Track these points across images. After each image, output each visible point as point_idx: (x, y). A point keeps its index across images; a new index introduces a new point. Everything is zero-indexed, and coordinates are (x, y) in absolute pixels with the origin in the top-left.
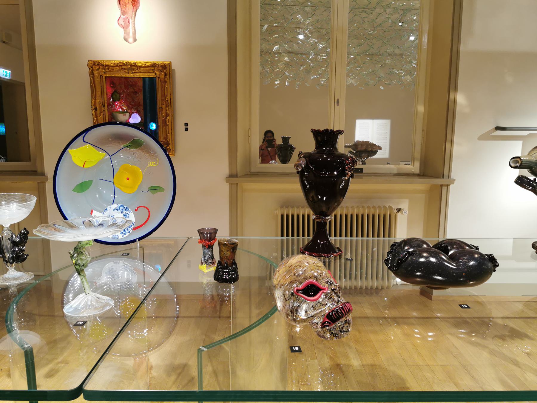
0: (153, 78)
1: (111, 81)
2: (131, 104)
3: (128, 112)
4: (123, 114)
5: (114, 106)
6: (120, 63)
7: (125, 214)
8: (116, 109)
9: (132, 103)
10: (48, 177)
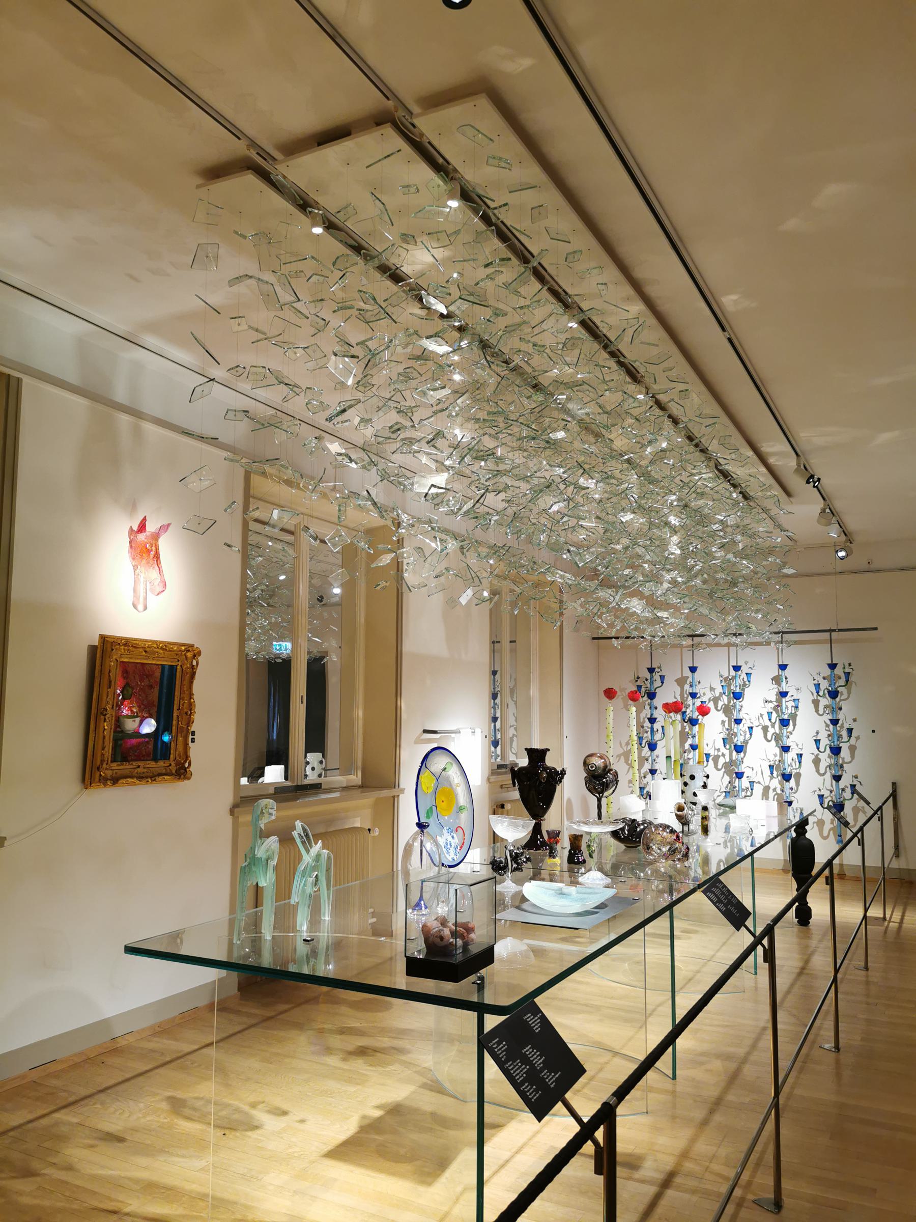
2: (142, 704)
9: (145, 703)
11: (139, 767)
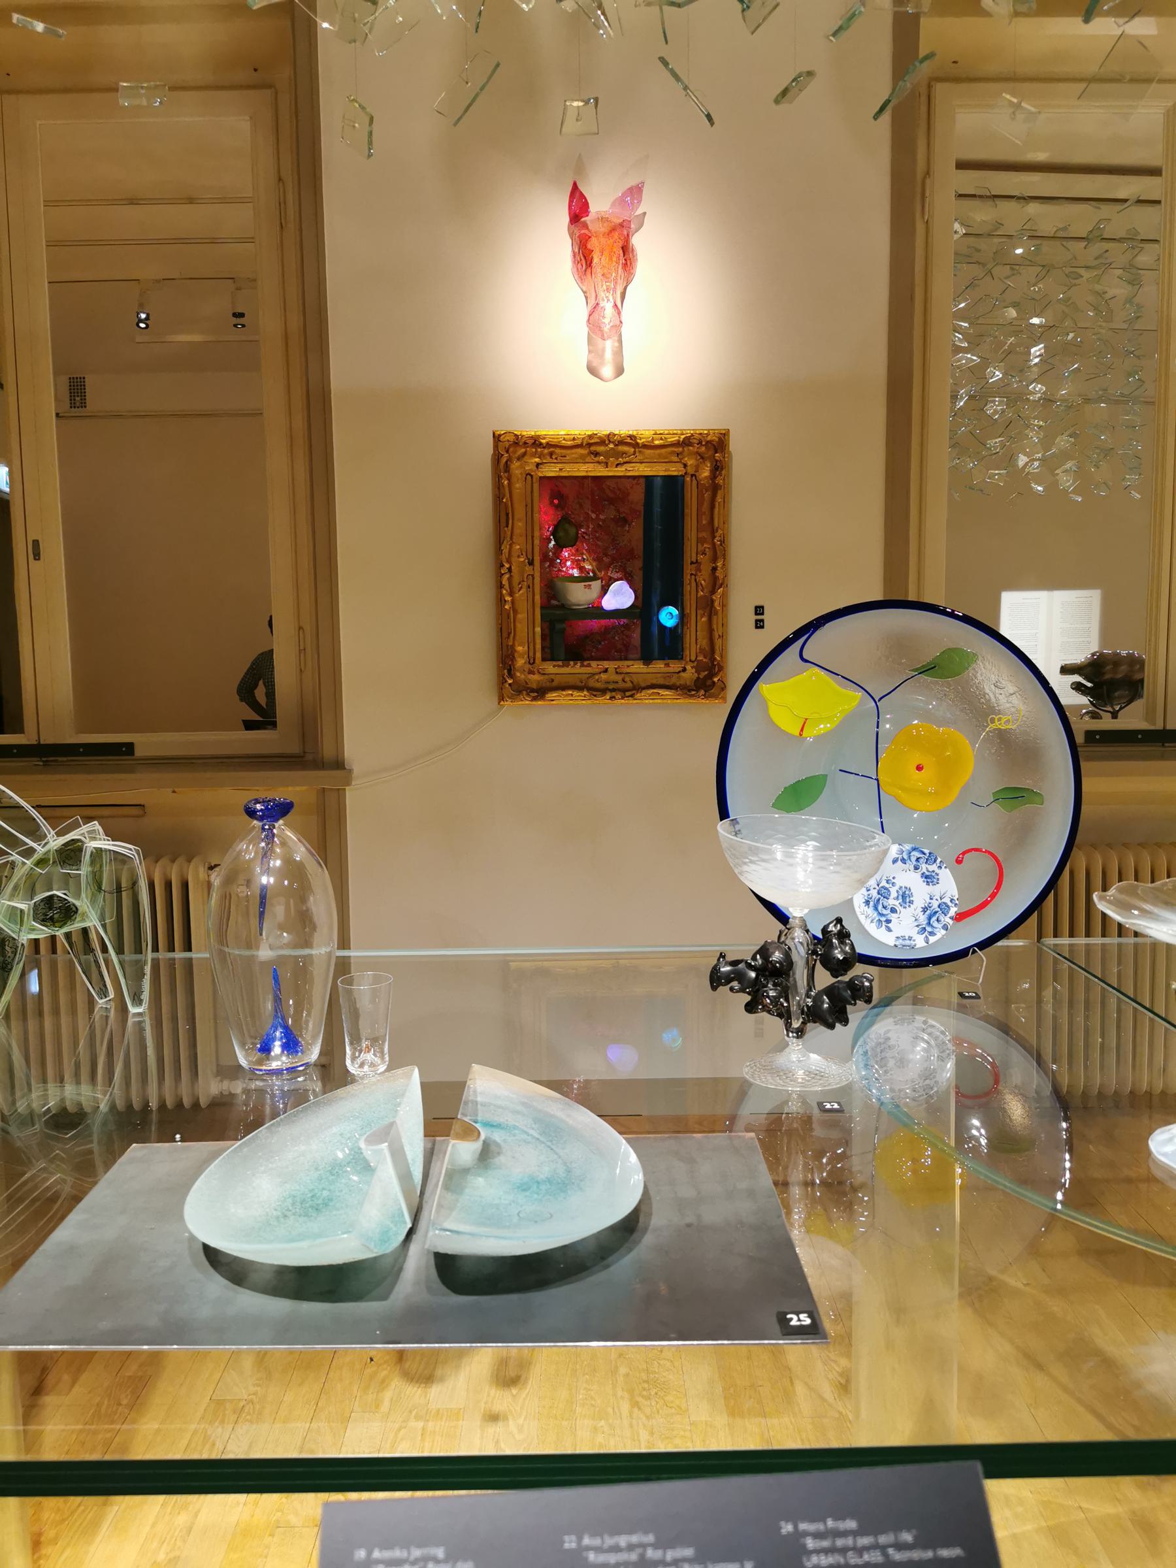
0: (677, 476)
1: (556, 489)
2: (606, 555)
3: (598, 579)
4: (583, 584)
5: (558, 561)
6: (590, 437)
7: (927, 873)
8: (564, 569)
9: (612, 552)
10: (350, 771)
11: (606, 671)
